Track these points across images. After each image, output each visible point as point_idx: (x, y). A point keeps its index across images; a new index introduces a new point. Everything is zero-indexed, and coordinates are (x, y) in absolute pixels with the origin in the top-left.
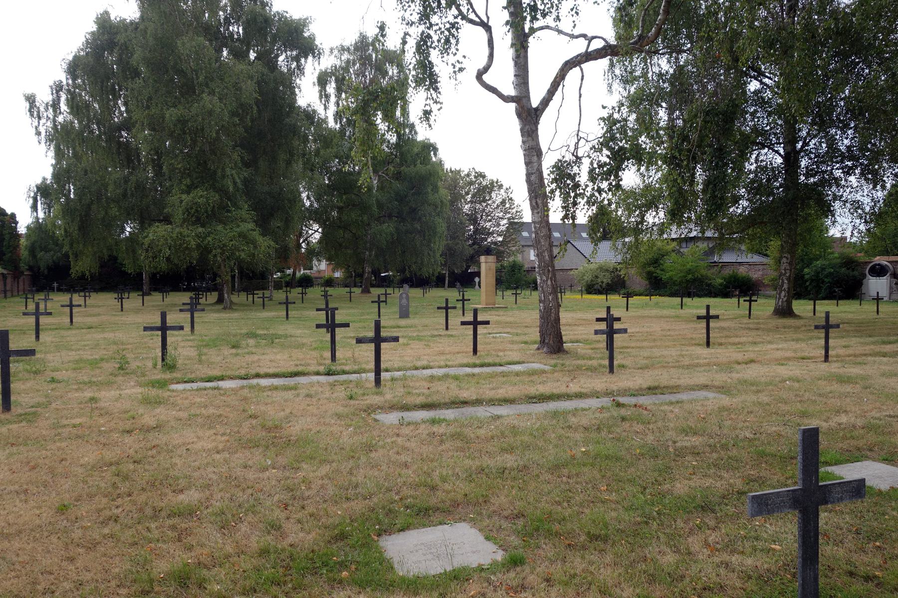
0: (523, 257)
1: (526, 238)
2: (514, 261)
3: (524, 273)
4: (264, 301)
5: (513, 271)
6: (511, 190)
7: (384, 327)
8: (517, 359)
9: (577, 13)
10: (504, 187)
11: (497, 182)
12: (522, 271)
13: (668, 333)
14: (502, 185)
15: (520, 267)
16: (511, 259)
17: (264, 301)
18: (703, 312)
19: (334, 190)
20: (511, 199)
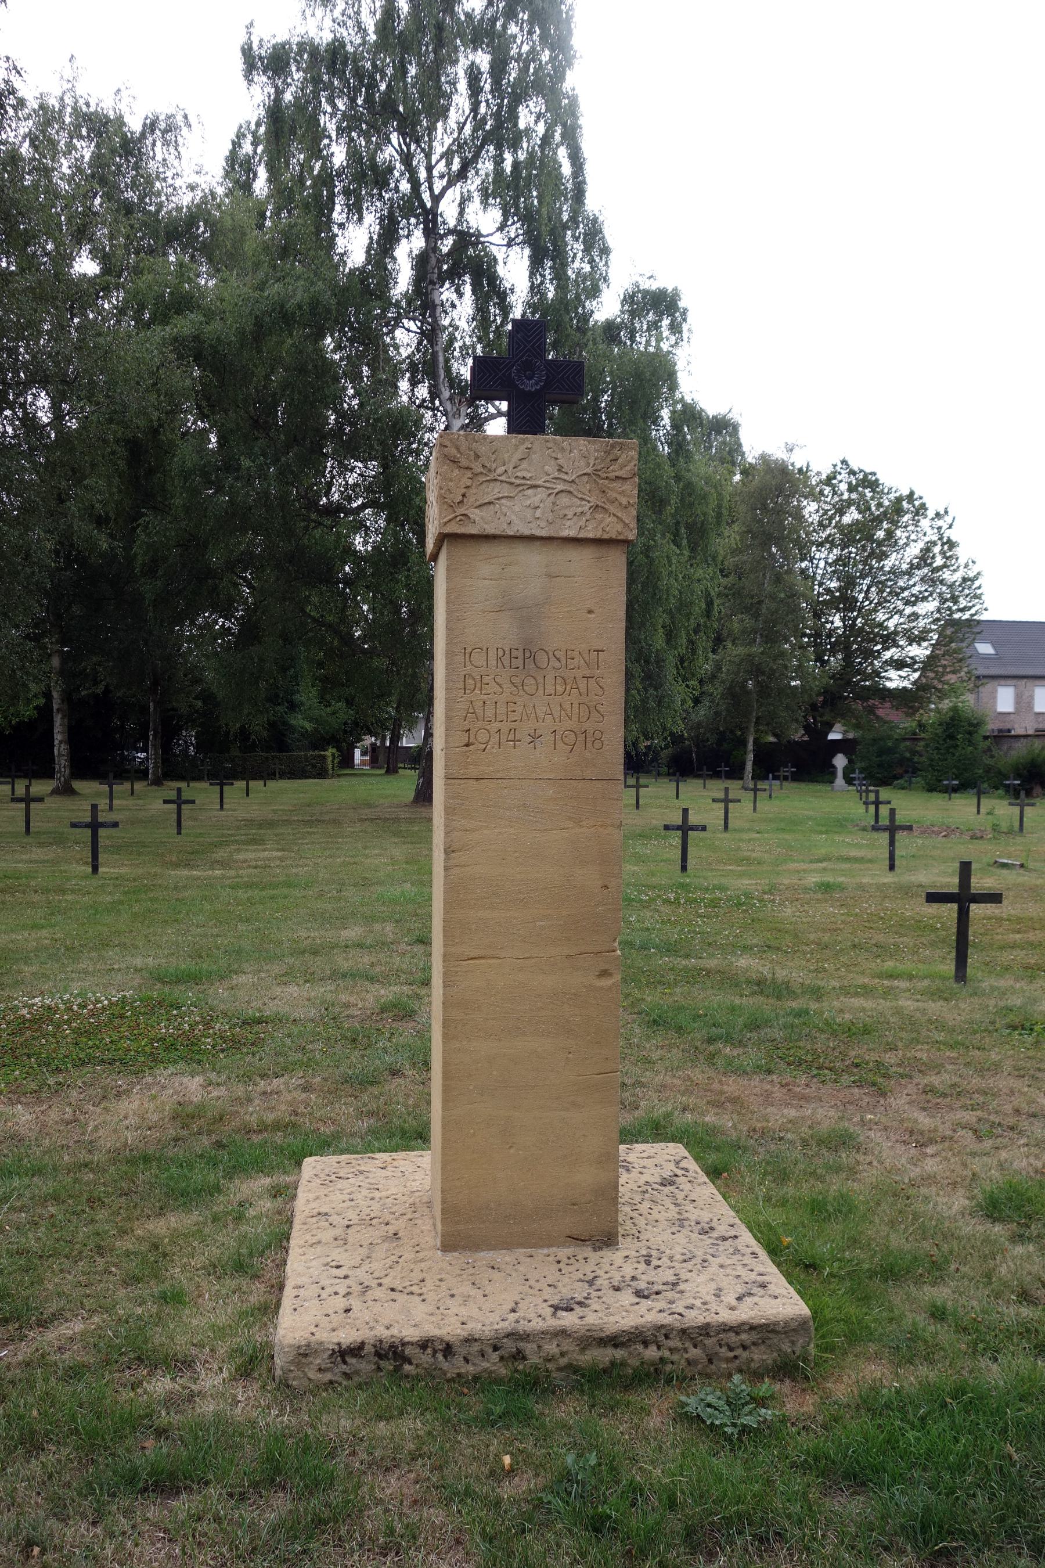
0: (978, 699)
1: (986, 657)
2: (955, 709)
3: (983, 745)
4: (963, 917)
5: (952, 737)
6: (948, 519)
7: (86, 863)
8: (476, 955)
9: (119, 90)
10: (931, 513)
11: (910, 497)
12: (978, 738)
13: (824, 864)
14: (923, 506)
15: (973, 726)
16: (946, 704)
17: (963, 917)
18: (721, 795)
19: (198, 358)
20: (951, 544)
